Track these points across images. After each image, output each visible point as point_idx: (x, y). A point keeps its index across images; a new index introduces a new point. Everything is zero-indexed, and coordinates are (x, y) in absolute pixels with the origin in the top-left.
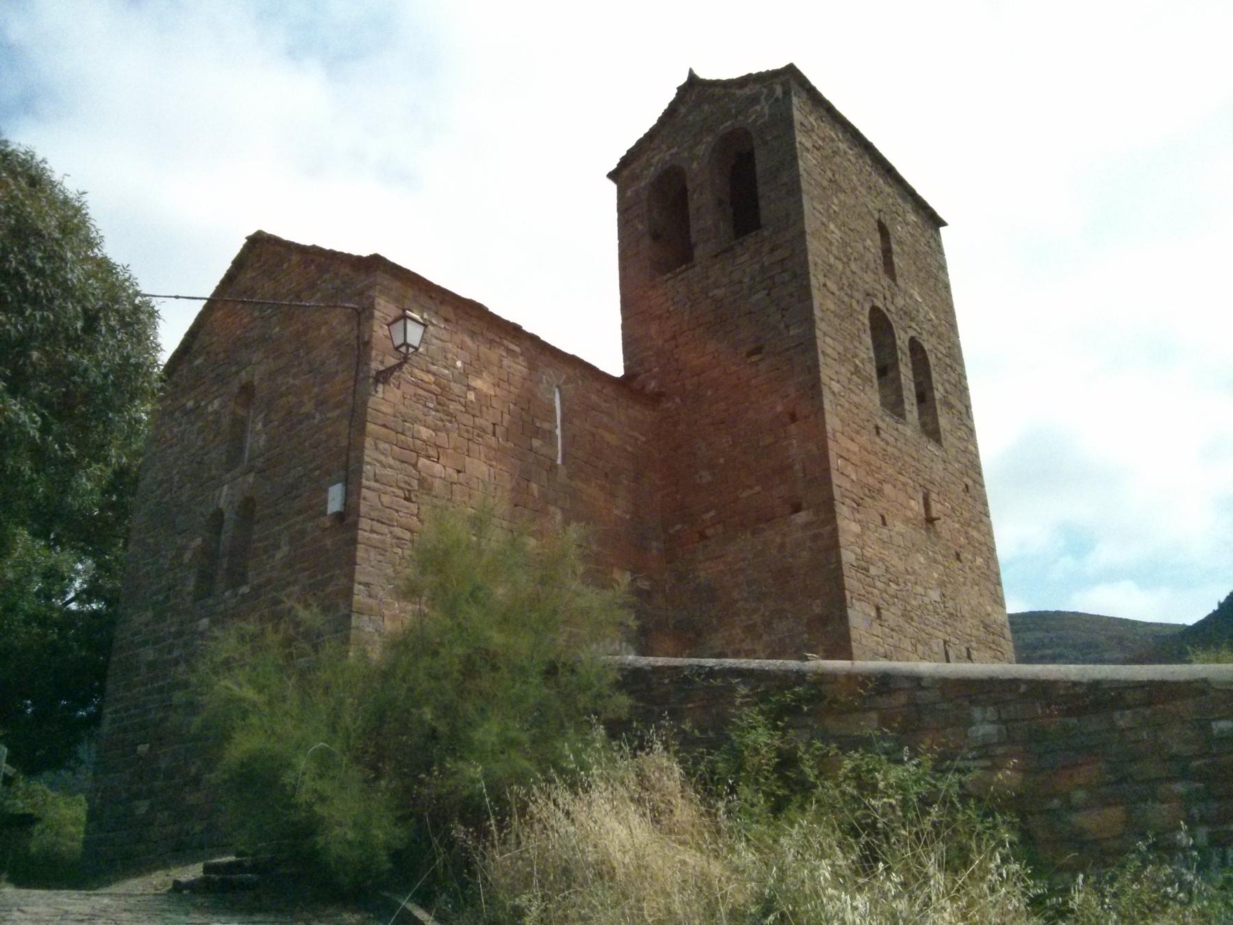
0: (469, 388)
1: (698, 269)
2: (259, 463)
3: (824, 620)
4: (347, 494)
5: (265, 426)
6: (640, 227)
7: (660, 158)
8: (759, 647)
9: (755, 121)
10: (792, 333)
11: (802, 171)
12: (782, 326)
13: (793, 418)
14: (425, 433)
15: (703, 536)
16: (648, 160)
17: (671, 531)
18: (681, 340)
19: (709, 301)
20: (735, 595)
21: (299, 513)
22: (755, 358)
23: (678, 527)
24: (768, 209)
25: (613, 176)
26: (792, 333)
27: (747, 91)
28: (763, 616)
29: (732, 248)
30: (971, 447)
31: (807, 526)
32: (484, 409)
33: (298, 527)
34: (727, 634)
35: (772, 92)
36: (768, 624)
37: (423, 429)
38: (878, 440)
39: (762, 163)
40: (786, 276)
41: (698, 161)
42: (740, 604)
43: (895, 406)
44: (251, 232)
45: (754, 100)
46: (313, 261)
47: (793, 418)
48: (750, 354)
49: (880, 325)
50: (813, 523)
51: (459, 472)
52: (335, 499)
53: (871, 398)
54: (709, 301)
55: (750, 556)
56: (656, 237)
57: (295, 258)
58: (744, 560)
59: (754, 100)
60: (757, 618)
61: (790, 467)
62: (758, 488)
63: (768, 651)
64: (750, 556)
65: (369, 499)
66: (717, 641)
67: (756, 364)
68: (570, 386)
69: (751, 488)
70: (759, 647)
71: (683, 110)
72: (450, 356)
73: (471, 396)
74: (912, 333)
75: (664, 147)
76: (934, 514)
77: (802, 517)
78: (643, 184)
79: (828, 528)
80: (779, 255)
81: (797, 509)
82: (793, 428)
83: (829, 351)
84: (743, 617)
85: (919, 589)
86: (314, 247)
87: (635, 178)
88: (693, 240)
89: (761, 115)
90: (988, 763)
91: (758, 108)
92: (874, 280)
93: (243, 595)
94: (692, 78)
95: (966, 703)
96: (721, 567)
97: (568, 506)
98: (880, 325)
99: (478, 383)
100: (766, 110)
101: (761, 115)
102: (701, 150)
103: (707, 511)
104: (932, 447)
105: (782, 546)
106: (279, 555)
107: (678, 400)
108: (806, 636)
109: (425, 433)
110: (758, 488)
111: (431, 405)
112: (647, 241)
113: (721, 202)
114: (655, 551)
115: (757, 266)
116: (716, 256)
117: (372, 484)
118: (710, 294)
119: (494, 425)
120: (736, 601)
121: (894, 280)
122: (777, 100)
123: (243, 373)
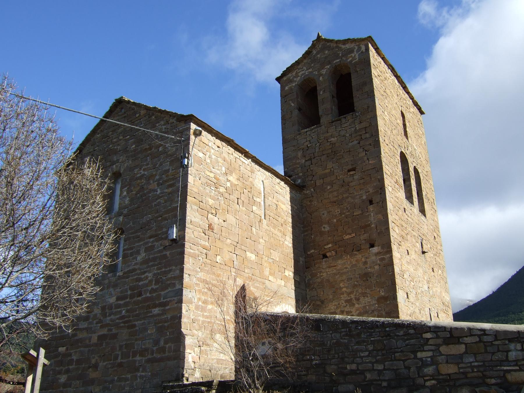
0: (228, 180)
1: (323, 127)
2: (125, 211)
3: (385, 298)
4: (178, 231)
5: (128, 193)
6: (293, 105)
7: (303, 72)
8: (353, 310)
9: (351, 61)
10: (370, 162)
11: (375, 87)
12: (366, 158)
13: (371, 202)
14: (211, 202)
15: (325, 256)
16: (296, 73)
17: (309, 253)
18: (314, 161)
19: (329, 144)
20: (342, 285)
21: (150, 237)
22: (352, 173)
23: (313, 251)
24: (358, 104)
25: (278, 79)
26: (370, 162)
27: (348, 46)
28: (355, 295)
29: (340, 120)
30: (436, 219)
31: (377, 254)
32: (234, 191)
33: (150, 244)
34: (337, 303)
35: (359, 48)
36: (358, 299)
37: (210, 200)
38: (405, 214)
39: (355, 82)
40: (368, 135)
41: (323, 78)
42: (344, 289)
43: (409, 197)
44: (118, 98)
45: (351, 51)
46: (153, 115)
47: (371, 202)
48: (349, 171)
49: (403, 158)
50: (381, 253)
51: (224, 221)
52: (174, 233)
53: (402, 194)
54: (329, 144)
55: (349, 267)
56: (300, 109)
57: (143, 112)
58: (346, 268)
59: (351, 51)
60: (352, 296)
61: (369, 225)
62: (353, 235)
63: (358, 312)
64: (349, 267)
65: (189, 234)
66: (332, 307)
67: (353, 175)
68: (267, 180)
69: (350, 234)
70: (353, 310)
71: (314, 52)
72: (220, 164)
73: (228, 184)
74: (415, 165)
75: (305, 68)
76: (425, 250)
77: (375, 250)
78: (294, 85)
79: (388, 255)
80: (363, 125)
81: (372, 246)
82: (371, 208)
83: (387, 172)
84: (345, 295)
85: (420, 285)
86: (175, 113)
87: (290, 81)
88: (320, 114)
89: (354, 58)
90: (517, 368)
91: (353, 55)
92: (401, 138)
93: (119, 276)
94: (319, 37)
95: (507, 342)
96: (335, 271)
97: (267, 240)
98: (403, 158)
99: (230, 178)
100: (357, 56)
101: (354, 58)
102: (324, 72)
103: (328, 244)
104: (423, 218)
105: (365, 263)
106: (139, 258)
107: (312, 190)
108: (377, 305)
109: (211, 202)
110: (353, 235)
111: (213, 188)
112: (296, 112)
113: (333, 97)
114: (301, 262)
115: (353, 129)
116: (332, 122)
117: (191, 226)
118: (329, 140)
119: (238, 199)
120: (342, 288)
121: (407, 139)
122: (362, 52)
123: (114, 166)
